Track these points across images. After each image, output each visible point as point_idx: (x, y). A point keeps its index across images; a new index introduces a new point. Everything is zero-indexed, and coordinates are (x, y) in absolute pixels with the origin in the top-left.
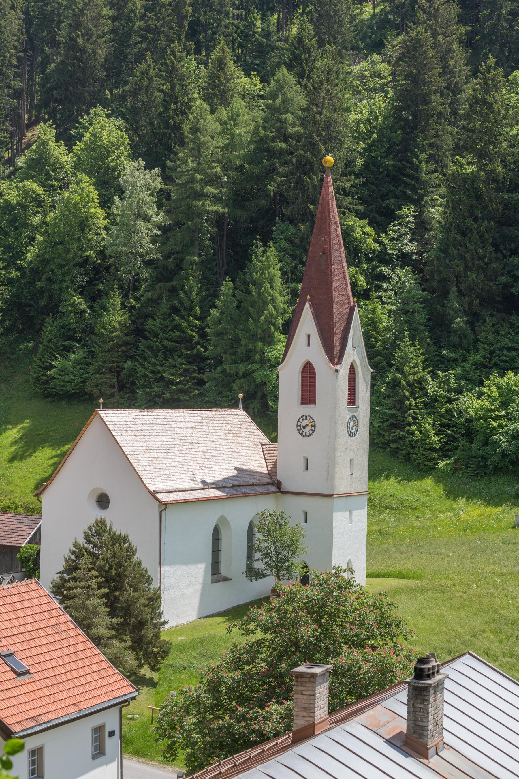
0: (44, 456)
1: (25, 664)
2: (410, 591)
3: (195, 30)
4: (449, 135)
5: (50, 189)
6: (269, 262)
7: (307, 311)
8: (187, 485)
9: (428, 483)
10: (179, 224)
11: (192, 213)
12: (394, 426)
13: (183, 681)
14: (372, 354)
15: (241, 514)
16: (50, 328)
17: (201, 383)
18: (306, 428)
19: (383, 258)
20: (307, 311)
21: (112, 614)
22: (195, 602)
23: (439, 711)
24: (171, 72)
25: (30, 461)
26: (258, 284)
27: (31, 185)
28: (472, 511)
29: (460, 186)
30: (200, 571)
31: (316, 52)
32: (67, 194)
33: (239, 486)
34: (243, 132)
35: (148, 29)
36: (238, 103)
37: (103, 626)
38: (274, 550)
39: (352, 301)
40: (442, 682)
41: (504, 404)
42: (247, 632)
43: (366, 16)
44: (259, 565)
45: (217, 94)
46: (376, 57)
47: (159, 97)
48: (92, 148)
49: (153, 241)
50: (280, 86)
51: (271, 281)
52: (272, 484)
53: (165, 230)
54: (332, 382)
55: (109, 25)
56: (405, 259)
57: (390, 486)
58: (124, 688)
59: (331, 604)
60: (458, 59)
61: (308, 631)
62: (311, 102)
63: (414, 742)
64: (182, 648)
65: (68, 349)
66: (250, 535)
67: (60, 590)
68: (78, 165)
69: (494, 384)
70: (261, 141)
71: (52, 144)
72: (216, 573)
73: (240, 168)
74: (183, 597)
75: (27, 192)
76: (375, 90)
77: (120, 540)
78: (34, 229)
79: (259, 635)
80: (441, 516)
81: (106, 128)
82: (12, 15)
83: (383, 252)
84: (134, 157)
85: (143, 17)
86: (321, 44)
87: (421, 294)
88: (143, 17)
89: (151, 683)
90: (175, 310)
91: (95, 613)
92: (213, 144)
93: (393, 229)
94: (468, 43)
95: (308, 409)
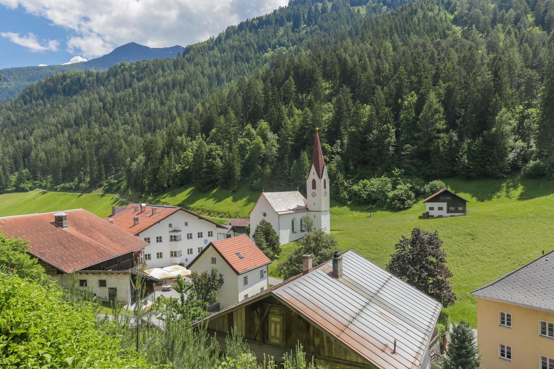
0: (252, 204)
1: (242, 256)
2: (341, 234)
3: (285, 99)
4: (348, 121)
5: (251, 140)
6: (305, 155)
7: (313, 167)
9: (345, 207)
10: (283, 147)
11: (286, 144)
12: (337, 194)
13: (283, 258)
14: (330, 176)
15: (299, 217)
16: (253, 174)
17: (289, 185)
18: (314, 195)
19: (333, 153)
20: (313, 167)
21: (267, 242)
22: (288, 238)
23: (342, 266)
24: (279, 110)
26: (303, 161)
27: (246, 139)
28: (357, 214)
29: (351, 134)
30: (289, 231)
31: (314, 103)
32: (255, 141)
33: (298, 210)
36: (296, 117)
37: (264, 245)
38: (306, 226)
39: (324, 163)
41: (364, 188)
42: (298, 245)
43: (327, 93)
44: (303, 229)
45: (290, 115)
46: (329, 103)
47: (276, 116)
48: (260, 129)
50: (306, 112)
51: (306, 160)
52: (306, 209)
53: (279, 149)
54: (320, 183)
56: (338, 153)
57: (336, 209)
58: (268, 260)
60: (350, 102)
63: (335, 274)
64: (285, 250)
66: (301, 221)
67: (254, 236)
68: (257, 134)
69: (361, 182)
71: (251, 129)
72: (293, 230)
73: (297, 133)
74: (285, 238)
75: (245, 141)
77: (268, 224)
78: (248, 150)
79: (301, 246)
80: (349, 215)
81: (264, 124)
83: (333, 151)
84: (270, 131)
85: (272, 96)
86: (316, 101)
88: (272, 96)
89: (277, 259)
90: (283, 168)
92: (290, 127)
93: (335, 145)
94: (353, 98)
95: (314, 190)
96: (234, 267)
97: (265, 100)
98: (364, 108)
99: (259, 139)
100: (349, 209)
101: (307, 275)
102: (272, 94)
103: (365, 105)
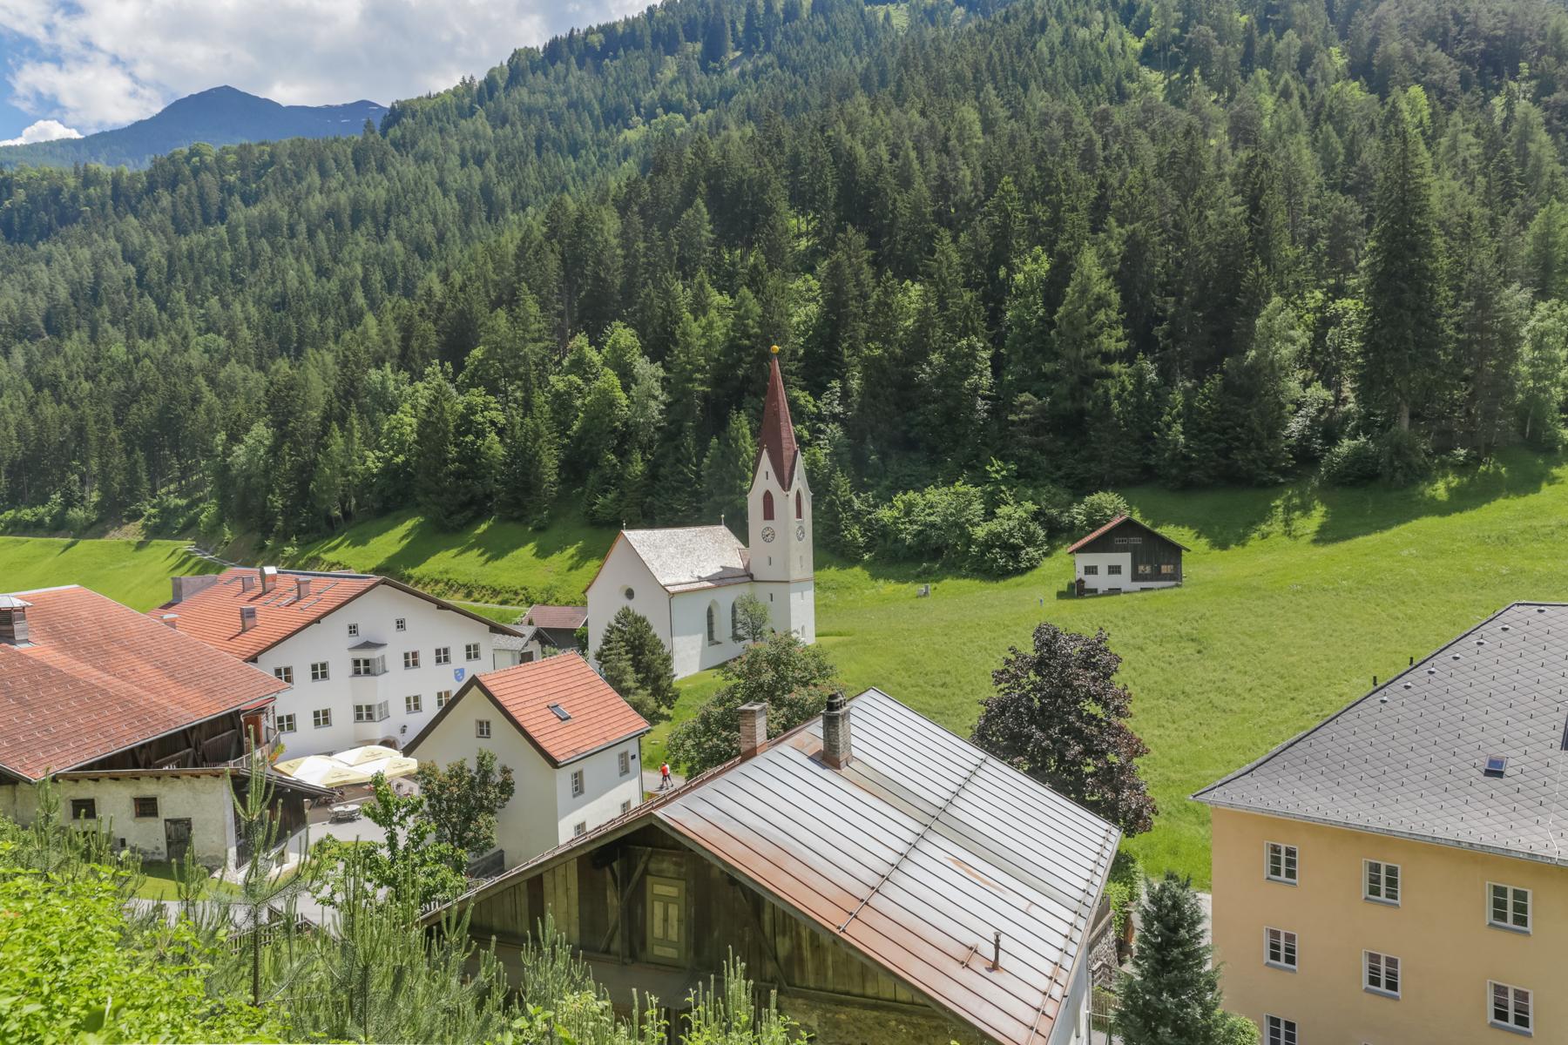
0: (592, 565)
4: (862, 328)
5: (587, 381)
6: (741, 424)
8: (688, 580)
9: (857, 570)
10: (677, 401)
13: (686, 716)
15: (726, 598)
16: (593, 477)
18: (768, 536)
19: (820, 417)
21: (637, 672)
22: (698, 659)
24: (667, 294)
25: (581, 571)
26: (736, 441)
27: (573, 378)
28: (888, 588)
29: (870, 365)
30: (699, 639)
33: (723, 579)
34: (718, 334)
35: (649, 264)
36: (713, 313)
37: (630, 681)
38: (749, 623)
39: (796, 446)
40: (848, 712)
41: (907, 514)
43: (802, 248)
44: (740, 632)
45: (699, 308)
46: (809, 276)
48: (614, 349)
49: (661, 412)
50: (743, 299)
51: (744, 437)
52: (748, 576)
54: (785, 503)
55: (621, 262)
56: (835, 417)
57: (832, 573)
58: (643, 724)
59: (784, 657)
60: (867, 274)
61: (768, 676)
62: (765, 310)
63: (829, 758)
64: (689, 692)
65: (606, 491)
66: (734, 612)
68: (605, 364)
69: (900, 499)
70: (732, 340)
71: (587, 349)
74: (688, 659)
75: (571, 383)
76: (809, 300)
77: (640, 620)
78: (577, 409)
79: (736, 681)
81: (623, 335)
82: (552, 256)
83: (820, 413)
84: (642, 355)
85: (645, 255)
86: (770, 269)
87: (847, 441)
88: (645, 255)
89: (668, 718)
90: (679, 461)
91: (624, 672)
93: (826, 396)
94: (873, 262)
95: (769, 523)
96: (544, 745)
97: (625, 266)
98: (905, 291)
99: (610, 378)
100: (867, 574)
101: (753, 761)
102: (648, 248)
103: (908, 282)
